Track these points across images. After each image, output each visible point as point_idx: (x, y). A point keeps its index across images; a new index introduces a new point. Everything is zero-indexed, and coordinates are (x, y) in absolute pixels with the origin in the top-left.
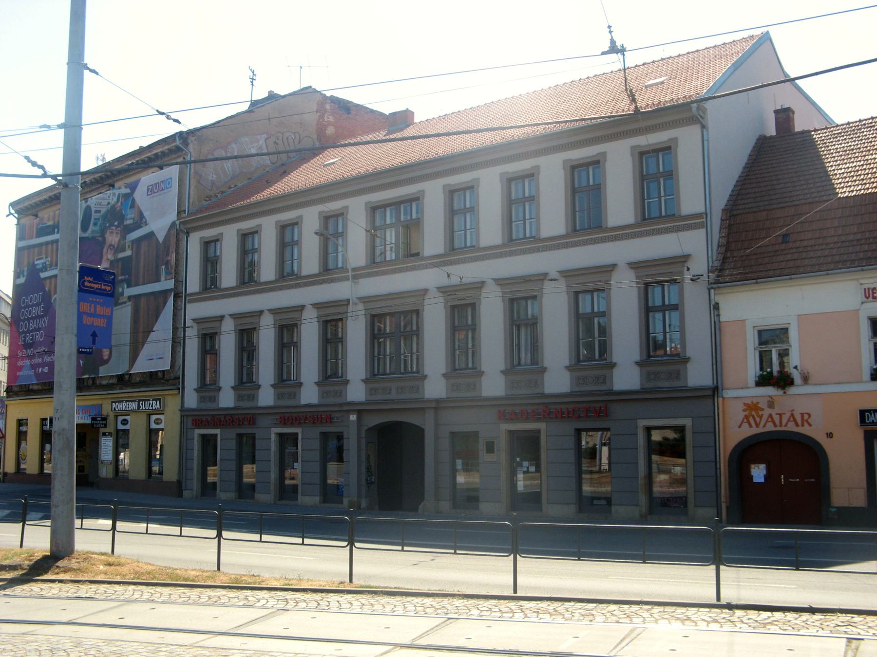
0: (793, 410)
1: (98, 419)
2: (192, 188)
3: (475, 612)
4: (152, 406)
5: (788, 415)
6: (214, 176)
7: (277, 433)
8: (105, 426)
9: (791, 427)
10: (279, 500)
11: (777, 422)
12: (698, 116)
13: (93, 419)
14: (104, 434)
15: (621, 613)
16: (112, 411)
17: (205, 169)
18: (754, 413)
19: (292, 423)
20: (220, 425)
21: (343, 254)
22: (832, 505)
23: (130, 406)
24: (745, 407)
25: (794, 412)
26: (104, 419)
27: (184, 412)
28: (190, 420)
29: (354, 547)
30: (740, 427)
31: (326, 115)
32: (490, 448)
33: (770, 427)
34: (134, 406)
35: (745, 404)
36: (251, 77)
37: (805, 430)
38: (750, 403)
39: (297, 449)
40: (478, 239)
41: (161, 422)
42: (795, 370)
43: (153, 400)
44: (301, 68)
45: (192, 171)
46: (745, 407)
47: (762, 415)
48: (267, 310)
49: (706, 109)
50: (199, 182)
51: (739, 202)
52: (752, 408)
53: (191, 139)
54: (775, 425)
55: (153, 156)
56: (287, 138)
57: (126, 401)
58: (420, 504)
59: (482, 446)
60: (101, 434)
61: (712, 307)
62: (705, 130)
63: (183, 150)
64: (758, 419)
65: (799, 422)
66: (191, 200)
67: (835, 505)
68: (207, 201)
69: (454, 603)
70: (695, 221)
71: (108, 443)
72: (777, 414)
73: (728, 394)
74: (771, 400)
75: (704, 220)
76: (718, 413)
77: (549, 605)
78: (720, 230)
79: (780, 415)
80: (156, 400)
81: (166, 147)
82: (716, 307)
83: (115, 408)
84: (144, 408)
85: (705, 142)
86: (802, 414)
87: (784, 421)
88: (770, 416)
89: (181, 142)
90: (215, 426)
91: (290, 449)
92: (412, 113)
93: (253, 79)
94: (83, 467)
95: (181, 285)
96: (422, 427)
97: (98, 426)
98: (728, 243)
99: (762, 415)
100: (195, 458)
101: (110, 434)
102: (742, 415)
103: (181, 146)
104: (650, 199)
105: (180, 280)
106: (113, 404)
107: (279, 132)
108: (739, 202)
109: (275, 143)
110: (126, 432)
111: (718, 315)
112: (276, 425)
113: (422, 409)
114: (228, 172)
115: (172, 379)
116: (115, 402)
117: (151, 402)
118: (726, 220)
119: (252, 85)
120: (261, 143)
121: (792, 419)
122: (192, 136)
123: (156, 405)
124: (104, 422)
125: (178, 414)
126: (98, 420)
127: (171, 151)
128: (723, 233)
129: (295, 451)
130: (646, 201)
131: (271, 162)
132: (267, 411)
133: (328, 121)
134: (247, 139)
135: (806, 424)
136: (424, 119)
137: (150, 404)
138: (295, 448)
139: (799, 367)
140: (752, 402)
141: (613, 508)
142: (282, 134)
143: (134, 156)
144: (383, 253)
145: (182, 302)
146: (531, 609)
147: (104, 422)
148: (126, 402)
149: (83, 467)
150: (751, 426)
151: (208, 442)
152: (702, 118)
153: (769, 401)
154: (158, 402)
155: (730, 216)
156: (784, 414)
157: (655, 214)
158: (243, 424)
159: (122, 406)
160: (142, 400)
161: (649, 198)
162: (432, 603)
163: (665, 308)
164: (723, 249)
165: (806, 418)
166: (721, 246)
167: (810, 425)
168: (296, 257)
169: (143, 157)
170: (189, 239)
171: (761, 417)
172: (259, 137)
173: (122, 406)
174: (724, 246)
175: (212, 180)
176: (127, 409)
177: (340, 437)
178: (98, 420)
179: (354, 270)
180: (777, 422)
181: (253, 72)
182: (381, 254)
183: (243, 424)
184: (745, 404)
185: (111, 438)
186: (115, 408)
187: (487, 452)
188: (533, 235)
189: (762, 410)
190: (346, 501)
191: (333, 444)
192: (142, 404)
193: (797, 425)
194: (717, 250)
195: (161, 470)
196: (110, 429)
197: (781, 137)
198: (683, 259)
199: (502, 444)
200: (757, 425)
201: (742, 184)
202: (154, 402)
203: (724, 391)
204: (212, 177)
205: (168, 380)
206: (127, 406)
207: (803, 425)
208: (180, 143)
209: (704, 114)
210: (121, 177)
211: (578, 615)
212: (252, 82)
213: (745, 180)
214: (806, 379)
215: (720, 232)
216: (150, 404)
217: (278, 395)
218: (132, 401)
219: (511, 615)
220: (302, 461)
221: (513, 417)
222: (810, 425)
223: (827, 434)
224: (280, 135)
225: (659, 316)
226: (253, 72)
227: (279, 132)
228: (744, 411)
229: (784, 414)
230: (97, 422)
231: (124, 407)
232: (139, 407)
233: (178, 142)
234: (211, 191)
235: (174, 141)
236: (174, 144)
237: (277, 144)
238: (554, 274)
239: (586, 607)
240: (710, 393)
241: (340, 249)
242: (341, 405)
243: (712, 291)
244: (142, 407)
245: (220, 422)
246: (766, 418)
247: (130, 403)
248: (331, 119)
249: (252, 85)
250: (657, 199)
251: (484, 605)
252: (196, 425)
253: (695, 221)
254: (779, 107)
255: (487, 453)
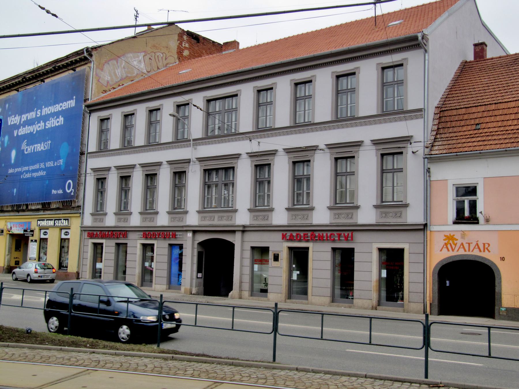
0: (478, 241)
1: (28, 231)
2: (94, 84)
3: (237, 377)
4: (63, 224)
5: (475, 243)
6: (109, 78)
7: (141, 244)
8: (33, 235)
9: (476, 252)
10: (141, 287)
11: (467, 249)
12: (422, 43)
13: (25, 231)
14: (32, 241)
15: (350, 384)
16: (37, 226)
17: (103, 73)
18: (451, 242)
19: (150, 237)
20: (105, 237)
21: (188, 130)
22: (503, 306)
23: (49, 223)
24: (445, 238)
25: (478, 242)
26: (32, 231)
27: (84, 229)
28: (86, 233)
29: (274, 311)
30: (441, 251)
31: (183, 43)
32: (276, 258)
33: (461, 252)
34: (51, 223)
35: (445, 236)
36: (136, 15)
37: (485, 255)
38: (449, 235)
39: (153, 254)
40: (274, 123)
41: (68, 234)
42: (480, 214)
43: (64, 219)
44: (169, 11)
45: (94, 73)
46: (445, 238)
47: (457, 243)
48: (139, 164)
49: (428, 39)
50: (98, 81)
51: (447, 102)
52: (450, 238)
53: (94, 53)
54: (465, 251)
55: (69, 63)
56: (158, 56)
57: (47, 220)
58: (230, 292)
59: (271, 256)
60: (30, 241)
61: (425, 171)
62: (426, 54)
63: (88, 60)
64: (453, 246)
65: (482, 249)
66: (93, 92)
67: (504, 306)
68: (104, 93)
69: (223, 369)
70: (418, 112)
71: (34, 247)
72: (467, 243)
73: (434, 228)
74: (463, 233)
75: (423, 113)
76: (427, 241)
77: (295, 374)
78: (433, 120)
79: (469, 244)
80: (66, 220)
81: (78, 57)
82: (428, 170)
83: (39, 224)
84: (58, 225)
85: (427, 62)
86: (484, 244)
87: (471, 248)
88: (462, 244)
89: (87, 54)
90: (102, 237)
91: (149, 254)
92: (238, 43)
93: (137, 16)
94: (19, 261)
95: (85, 146)
96: (233, 242)
97: (27, 235)
98: (438, 129)
99: (457, 243)
100: (89, 258)
101: (36, 241)
102: (442, 243)
103: (87, 56)
104: (387, 99)
105: (84, 143)
106: (39, 221)
107: (153, 52)
108: (447, 102)
109: (150, 59)
110: (46, 239)
111: (430, 176)
112: (140, 239)
113: (234, 232)
114: (118, 76)
115: (76, 207)
116: (40, 220)
117: (62, 221)
118: (438, 114)
119: (136, 20)
120: (140, 58)
121: (477, 247)
122: (95, 51)
123: (65, 223)
124: (32, 233)
125: (79, 229)
126: (28, 232)
127: (81, 60)
128: (435, 122)
129: (152, 255)
130: (385, 100)
131: (147, 71)
132: (135, 230)
133: (185, 47)
134: (131, 55)
135: (486, 250)
136: (245, 47)
137: (61, 222)
138: (152, 253)
139: (483, 213)
140: (450, 234)
141: (355, 301)
142: (155, 53)
143: (58, 62)
144: (213, 131)
145: (84, 157)
146: (281, 377)
147: (32, 233)
148: (46, 221)
149: (19, 261)
150: (448, 250)
151: (98, 248)
152: (426, 45)
153: (462, 234)
154: (67, 221)
155: (440, 112)
156: (472, 243)
157: (390, 108)
158: (120, 237)
159: (44, 223)
160: (57, 220)
161: (387, 98)
162: (207, 368)
163: (394, 171)
164: (435, 133)
165: (486, 247)
166: (433, 131)
167: (489, 251)
168: (158, 131)
169: (63, 63)
170: (90, 117)
171: (456, 245)
172: (139, 54)
173: (44, 223)
174: (435, 131)
175: (107, 80)
176: (47, 225)
177: (181, 247)
178: (28, 232)
179: (194, 140)
180: (467, 249)
181: (137, 12)
182: (212, 131)
183: (120, 237)
184: (445, 236)
185: (36, 244)
186: (39, 224)
187: (274, 261)
188: (310, 121)
189: (457, 240)
190: (183, 289)
191: (176, 251)
192: (57, 222)
193: (480, 251)
194: (431, 133)
195: (67, 265)
196: (36, 237)
197: (477, 61)
198: (407, 139)
199: (284, 255)
200: (453, 250)
201: (450, 91)
202: (65, 221)
203: (431, 226)
204: (108, 78)
205: (74, 207)
206: (47, 223)
207: (484, 251)
208: (87, 55)
209: (427, 42)
210: (49, 76)
211: (316, 383)
212: (136, 18)
213: (451, 88)
214: (487, 221)
215: (433, 122)
216: (61, 222)
217: (143, 219)
218: (50, 220)
219: (264, 381)
220: (156, 262)
221: (291, 239)
222: (489, 251)
223: (501, 258)
224: (153, 54)
225: (390, 175)
226: (137, 12)
227: (153, 52)
228: (444, 240)
229: (472, 243)
230: (27, 233)
231: (45, 223)
232: (55, 224)
233: (86, 54)
234: (106, 87)
235: (83, 53)
236: (83, 55)
237: (151, 60)
238: (322, 146)
239: (324, 377)
240: (422, 227)
241: (186, 127)
242: (182, 227)
243: (426, 160)
244: (57, 224)
245: (105, 235)
246: (459, 246)
247: (49, 221)
248: (187, 45)
249: (136, 20)
250: (392, 99)
251: (246, 372)
252: (90, 237)
253: (418, 112)
254: (476, 42)
255: (274, 261)
